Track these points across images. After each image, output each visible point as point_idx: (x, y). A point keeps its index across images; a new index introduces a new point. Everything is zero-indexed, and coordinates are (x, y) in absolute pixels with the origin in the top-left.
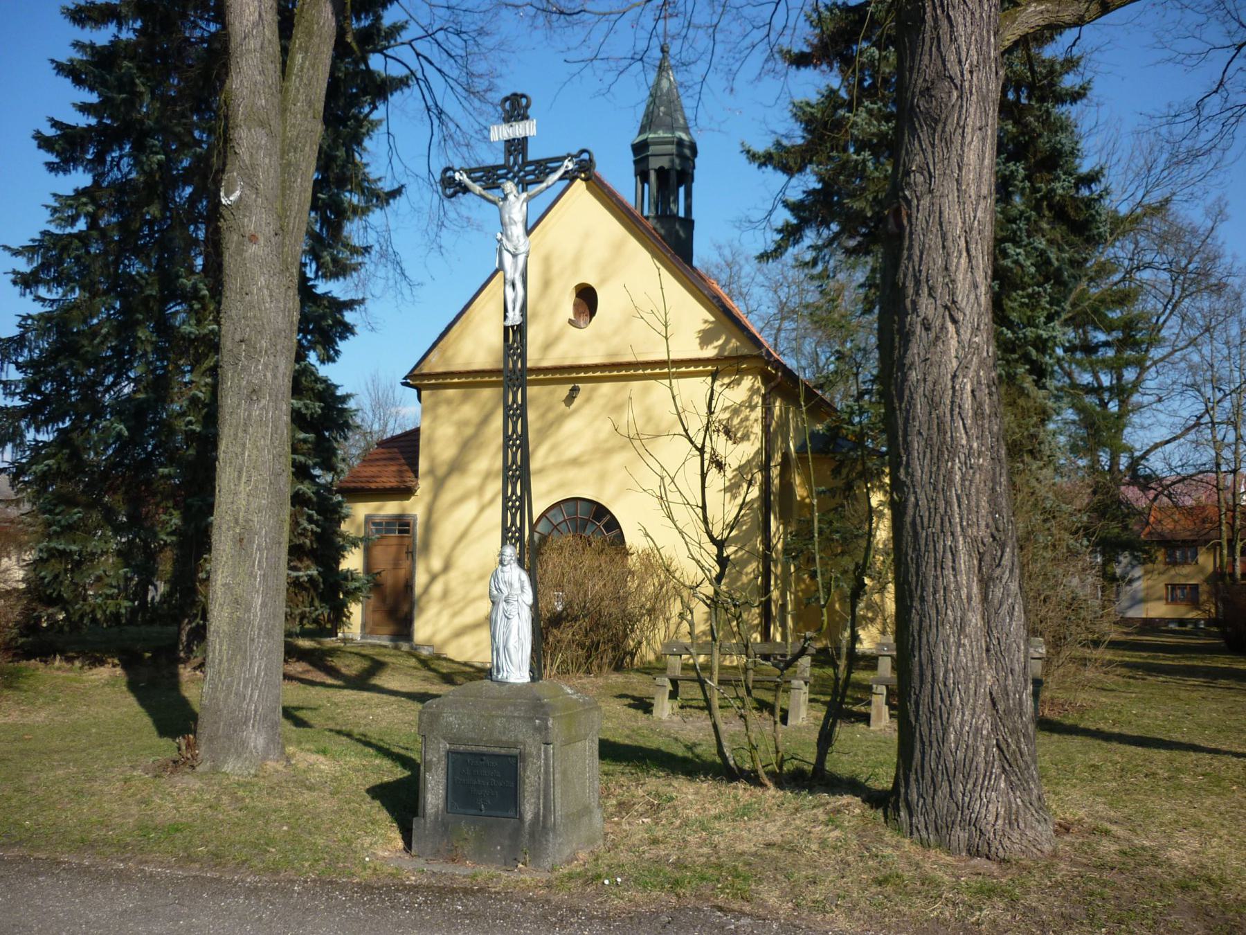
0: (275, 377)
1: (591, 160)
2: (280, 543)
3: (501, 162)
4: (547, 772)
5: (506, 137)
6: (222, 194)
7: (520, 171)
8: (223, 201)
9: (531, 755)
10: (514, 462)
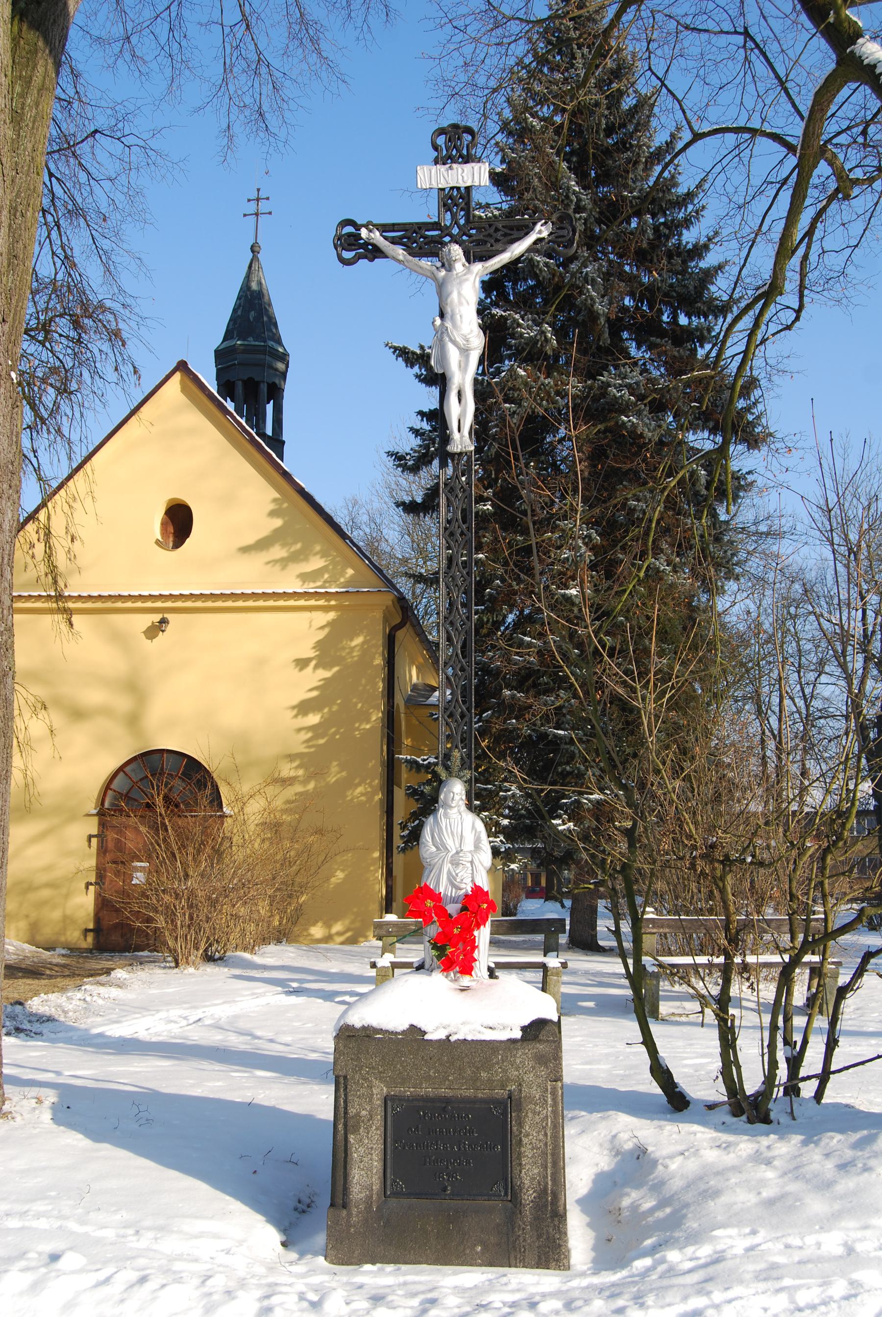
9: (530, 1098)
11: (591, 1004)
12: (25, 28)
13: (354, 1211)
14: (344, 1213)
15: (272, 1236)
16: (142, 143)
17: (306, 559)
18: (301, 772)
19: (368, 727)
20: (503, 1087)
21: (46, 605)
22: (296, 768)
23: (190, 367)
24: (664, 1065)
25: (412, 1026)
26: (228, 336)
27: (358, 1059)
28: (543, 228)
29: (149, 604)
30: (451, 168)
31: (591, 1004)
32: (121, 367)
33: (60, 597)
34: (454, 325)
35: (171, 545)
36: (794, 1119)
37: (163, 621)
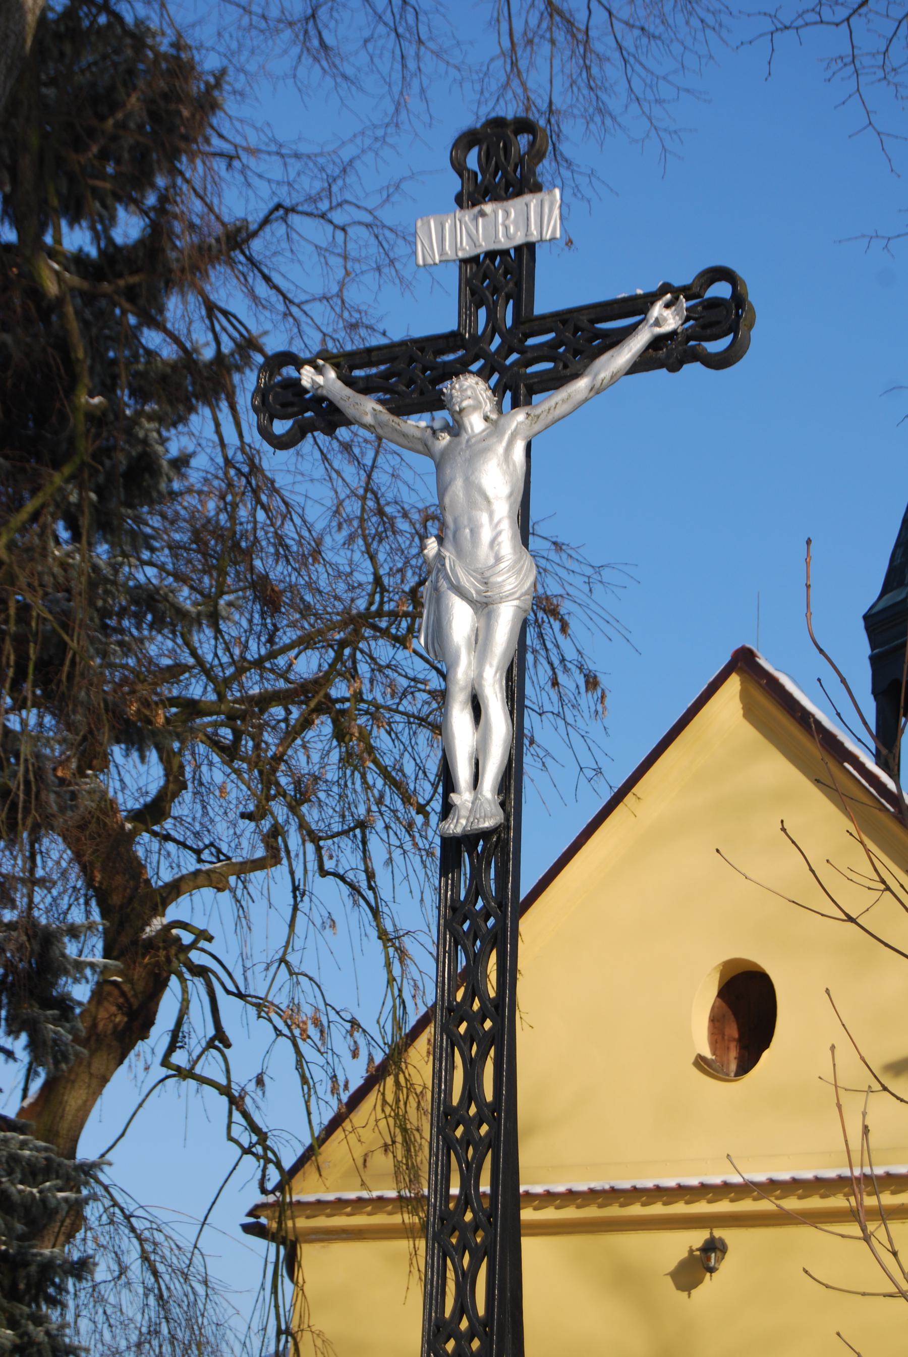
1: (739, 300)
5: (467, 250)
10: (464, 1305)
16: (368, 218)
21: (397, 1219)
23: (762, 662)
28: (667, 313)
29: (680, 1208)
30: (482, 214)
32: (562, 678)
34: (459, 552)
35: (733, 1067)
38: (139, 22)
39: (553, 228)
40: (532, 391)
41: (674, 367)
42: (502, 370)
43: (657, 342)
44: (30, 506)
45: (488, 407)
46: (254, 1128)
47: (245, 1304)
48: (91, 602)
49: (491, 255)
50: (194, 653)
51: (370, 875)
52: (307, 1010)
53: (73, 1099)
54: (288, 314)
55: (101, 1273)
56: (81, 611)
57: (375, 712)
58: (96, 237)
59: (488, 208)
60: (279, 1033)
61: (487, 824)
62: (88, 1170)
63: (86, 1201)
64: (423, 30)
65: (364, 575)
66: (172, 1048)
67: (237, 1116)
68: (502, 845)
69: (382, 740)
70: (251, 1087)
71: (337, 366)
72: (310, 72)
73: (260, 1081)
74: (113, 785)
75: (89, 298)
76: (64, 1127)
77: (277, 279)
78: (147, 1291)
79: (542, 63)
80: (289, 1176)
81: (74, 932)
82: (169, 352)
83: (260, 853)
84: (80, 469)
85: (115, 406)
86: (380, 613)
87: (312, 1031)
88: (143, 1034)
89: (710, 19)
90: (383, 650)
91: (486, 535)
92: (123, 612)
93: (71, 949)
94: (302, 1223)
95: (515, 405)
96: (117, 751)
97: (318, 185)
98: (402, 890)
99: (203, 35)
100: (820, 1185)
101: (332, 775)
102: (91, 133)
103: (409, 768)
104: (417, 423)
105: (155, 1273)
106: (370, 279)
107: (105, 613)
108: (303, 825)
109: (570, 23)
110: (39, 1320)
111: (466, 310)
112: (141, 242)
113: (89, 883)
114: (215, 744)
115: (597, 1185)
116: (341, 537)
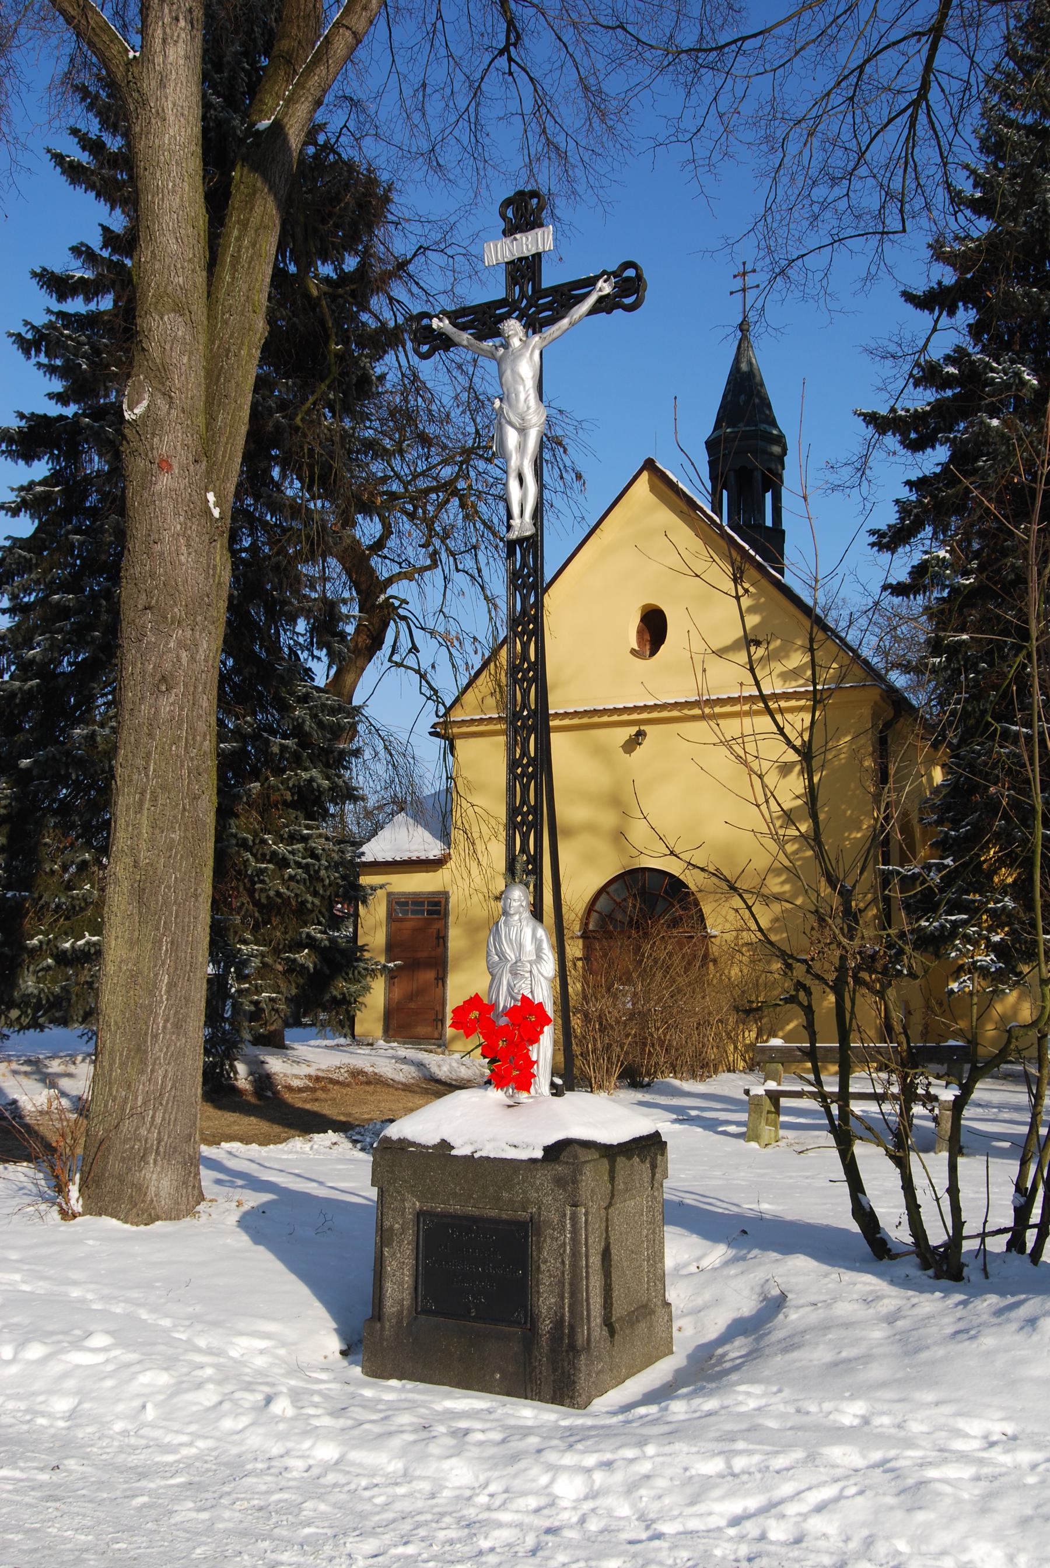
0: (193, 659)
1: (639, 277)
2: (196, 896)
3: (500, 294)
4: (575, 1254)
6: (125, 407)
7: (529, 306)
8: (127, 417)
9: (549, 1223)
11: (1007, 1145)
12: (246, 170)
13: (387, 1325)
14: (378, 1325)
15: (334, 1344)
16: (464, 251)
17: (787, 656)
18: (787, 887)
19: (859, 835)
20: (524, 1210)
22: (783, 883)
24: (866, 1206)
25: (443, 1141)
26: (717, 426)
27: (393, 1172)
29: (625, 717)
31: (1007, 1145)
32: (565, 475)
33: (770, 713)
34: (510, 405)
36: (987, 1277)
37: (640, 734)
38: (351, 159)
39: (549, 245)
40: (542, 326)
41: (609, 312)
42: (528, 316)
43: (601, 299)
44: (311, 399)
45: (521, 334)
46: (431, 688)
47: (432, 767)
48: (343, 446)
49: (520, 259)
50: (393, 470)
51: (479, 571)
52: (453, 633)
53: (349, 678)
54: (428, 301)
55: (367, 754)
56: (337, 448)
57: (479, 495)
58: (335, 269)
59: (518, 236)
60: (441, 645)
61: (528, 534)
62: (358, 710)
63: (357, 723)
64: (486, 154)
65: (471, 429)
66: (392, 654)
67: (424, 683)
68: (535, 543)
69: (482, 508)
70: (429, 669)
71: (449, 318)
72: (433, 178)
73: (433, 667)
74: (358, 534)
75: (334, 298)
76: (346, 691)
77: (422, 284)
78: (388, 763)
79: (545, 170)
80: (448, 710)
81: (344, 601)
82: (373, 324)
83: (428, 562)
84: (333, 382)
85: (348, 351)
86: (479, 447)
87: (456, 643)
88: (380, 649)
89: (625, 144)
90: (481, 465)
91: (522, 396)
92: (358, 452)
93: (344, 610)
94: (456, 730)
95: (534, 333)
96: (360, 517)
97: (439, 236)
98: (494, 577)
99: (381, 162)
100: (687, 704)
101: (460, 523)
102: (330, 215)
103: (496, 520)
104: (488, 344)
105: (391, 755)
106: (466, 281)
107: (350, 452)
108: (447, 549)
109: (557, 148)
110: (340, 776)
111: (509, 288)
112: (356, 270)
113: (350, 578)
114: (405, 512)
115: (587, 708)
116: (459, 411)
